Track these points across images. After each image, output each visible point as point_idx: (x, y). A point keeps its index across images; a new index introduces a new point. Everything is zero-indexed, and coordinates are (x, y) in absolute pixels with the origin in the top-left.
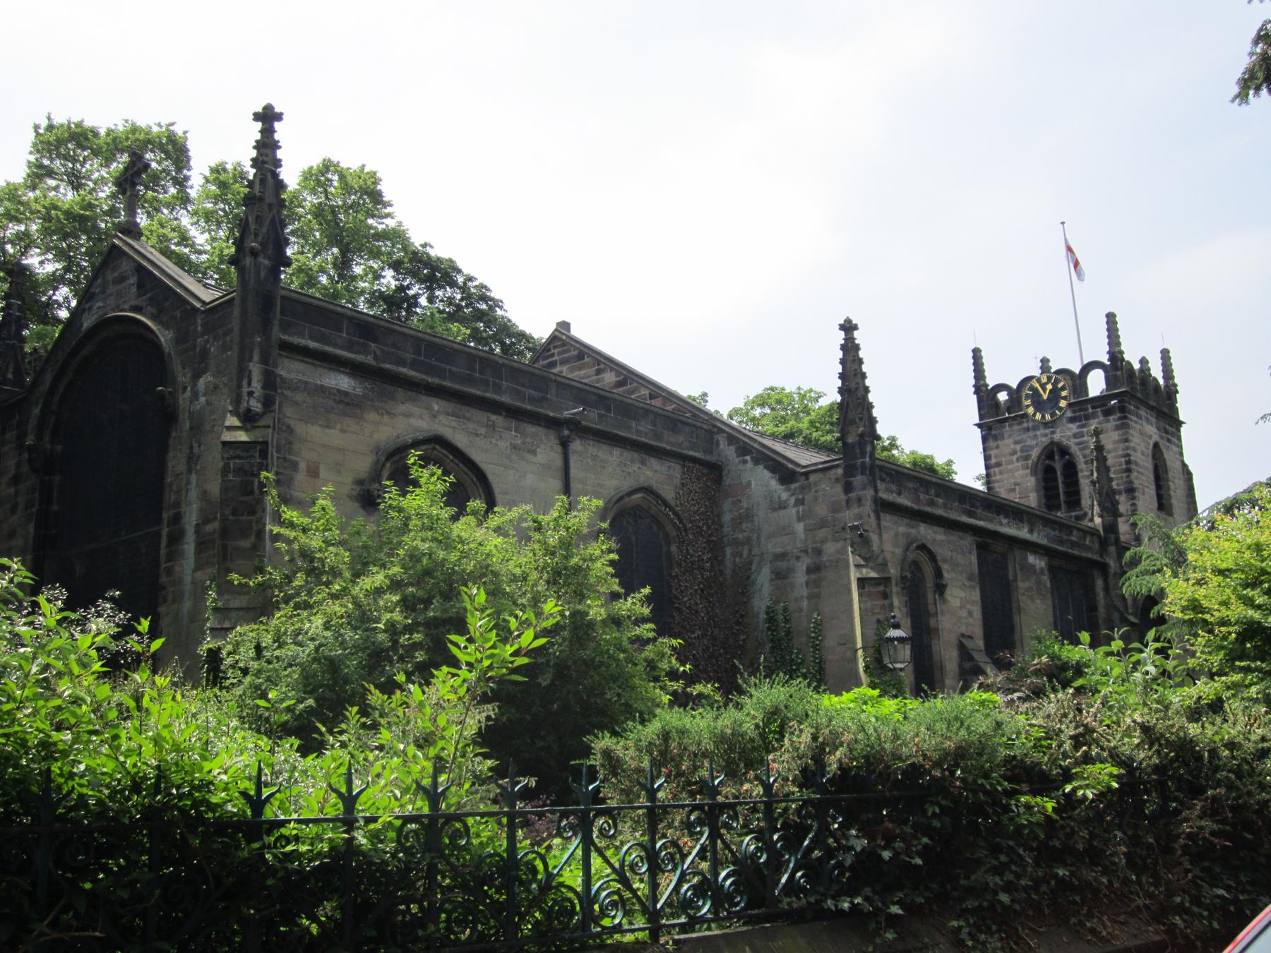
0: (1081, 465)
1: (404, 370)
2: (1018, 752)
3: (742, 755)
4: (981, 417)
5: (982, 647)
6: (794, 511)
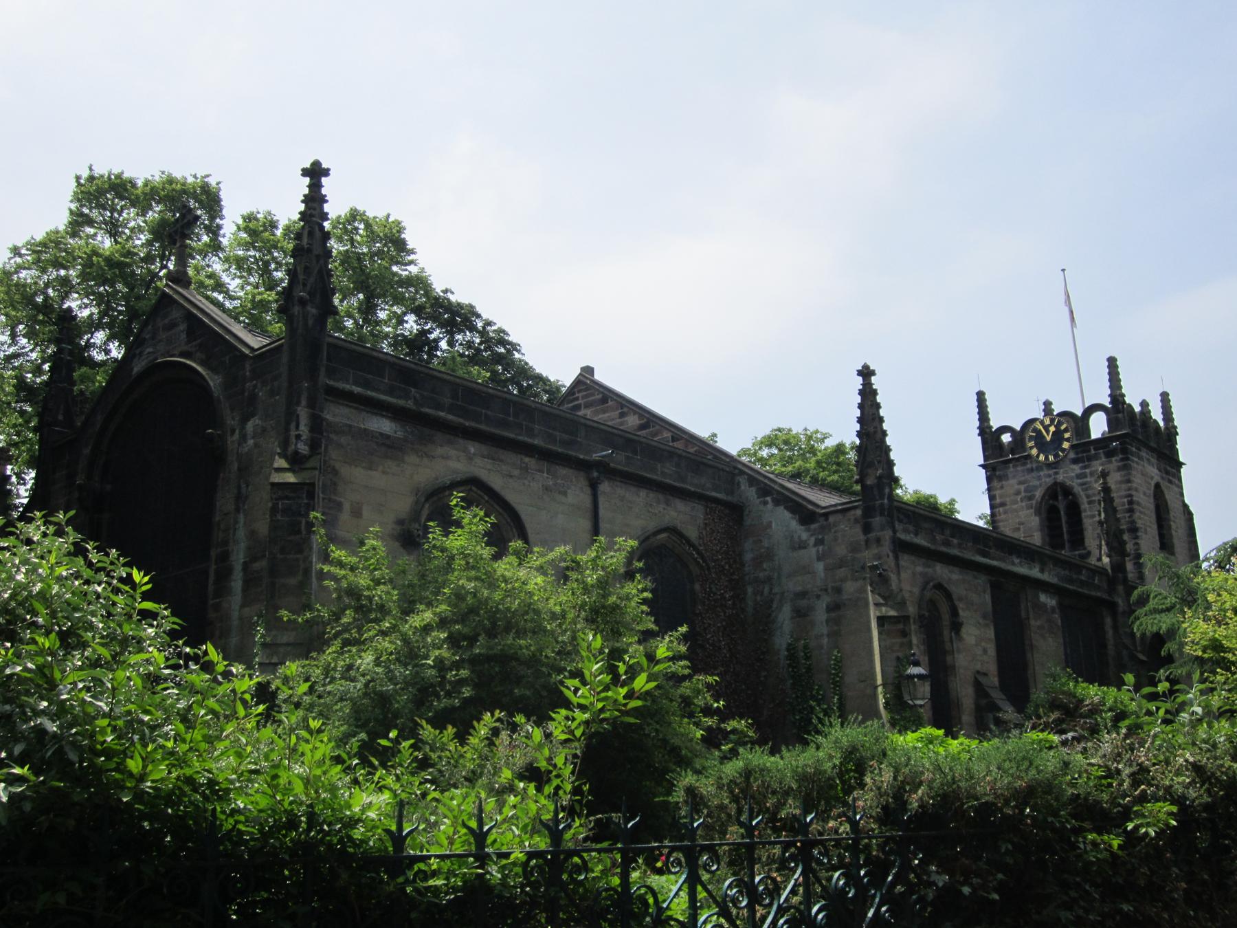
0: (1084, 505)
1: (442, 414)
2: (1082, 791)
3: (821, 793)
4: (986, 458)
5: (997, 683)
6: (814, 550)
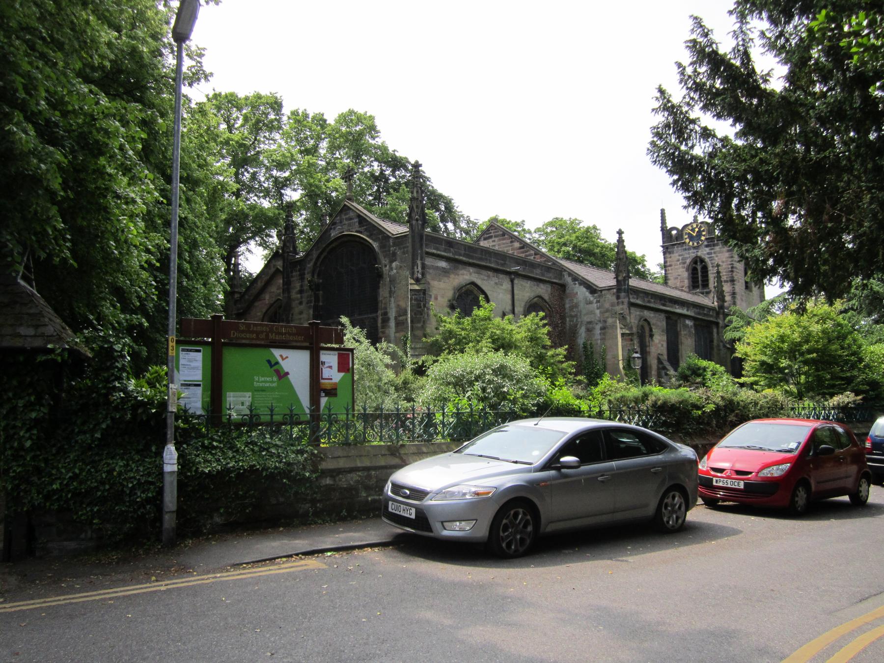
0: (710, 268)
4: (664, 242)
